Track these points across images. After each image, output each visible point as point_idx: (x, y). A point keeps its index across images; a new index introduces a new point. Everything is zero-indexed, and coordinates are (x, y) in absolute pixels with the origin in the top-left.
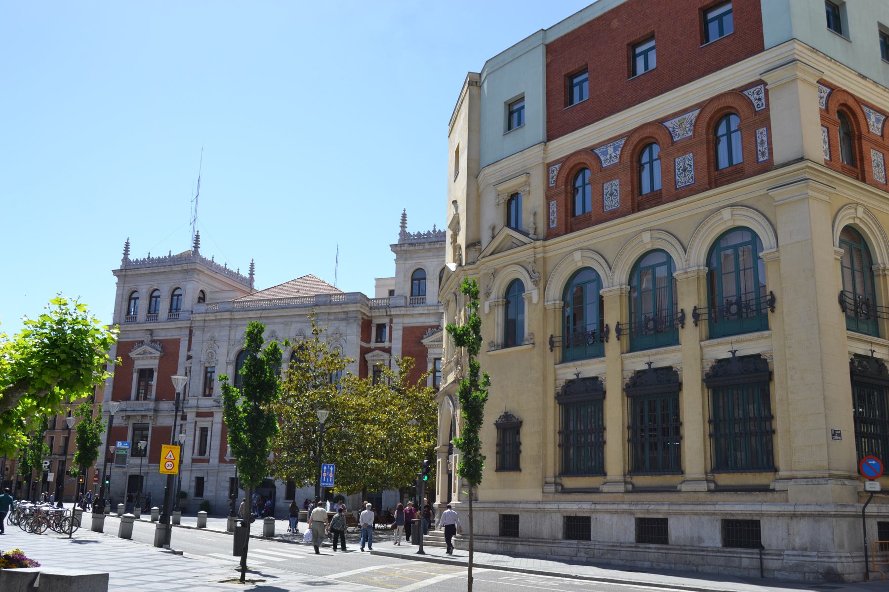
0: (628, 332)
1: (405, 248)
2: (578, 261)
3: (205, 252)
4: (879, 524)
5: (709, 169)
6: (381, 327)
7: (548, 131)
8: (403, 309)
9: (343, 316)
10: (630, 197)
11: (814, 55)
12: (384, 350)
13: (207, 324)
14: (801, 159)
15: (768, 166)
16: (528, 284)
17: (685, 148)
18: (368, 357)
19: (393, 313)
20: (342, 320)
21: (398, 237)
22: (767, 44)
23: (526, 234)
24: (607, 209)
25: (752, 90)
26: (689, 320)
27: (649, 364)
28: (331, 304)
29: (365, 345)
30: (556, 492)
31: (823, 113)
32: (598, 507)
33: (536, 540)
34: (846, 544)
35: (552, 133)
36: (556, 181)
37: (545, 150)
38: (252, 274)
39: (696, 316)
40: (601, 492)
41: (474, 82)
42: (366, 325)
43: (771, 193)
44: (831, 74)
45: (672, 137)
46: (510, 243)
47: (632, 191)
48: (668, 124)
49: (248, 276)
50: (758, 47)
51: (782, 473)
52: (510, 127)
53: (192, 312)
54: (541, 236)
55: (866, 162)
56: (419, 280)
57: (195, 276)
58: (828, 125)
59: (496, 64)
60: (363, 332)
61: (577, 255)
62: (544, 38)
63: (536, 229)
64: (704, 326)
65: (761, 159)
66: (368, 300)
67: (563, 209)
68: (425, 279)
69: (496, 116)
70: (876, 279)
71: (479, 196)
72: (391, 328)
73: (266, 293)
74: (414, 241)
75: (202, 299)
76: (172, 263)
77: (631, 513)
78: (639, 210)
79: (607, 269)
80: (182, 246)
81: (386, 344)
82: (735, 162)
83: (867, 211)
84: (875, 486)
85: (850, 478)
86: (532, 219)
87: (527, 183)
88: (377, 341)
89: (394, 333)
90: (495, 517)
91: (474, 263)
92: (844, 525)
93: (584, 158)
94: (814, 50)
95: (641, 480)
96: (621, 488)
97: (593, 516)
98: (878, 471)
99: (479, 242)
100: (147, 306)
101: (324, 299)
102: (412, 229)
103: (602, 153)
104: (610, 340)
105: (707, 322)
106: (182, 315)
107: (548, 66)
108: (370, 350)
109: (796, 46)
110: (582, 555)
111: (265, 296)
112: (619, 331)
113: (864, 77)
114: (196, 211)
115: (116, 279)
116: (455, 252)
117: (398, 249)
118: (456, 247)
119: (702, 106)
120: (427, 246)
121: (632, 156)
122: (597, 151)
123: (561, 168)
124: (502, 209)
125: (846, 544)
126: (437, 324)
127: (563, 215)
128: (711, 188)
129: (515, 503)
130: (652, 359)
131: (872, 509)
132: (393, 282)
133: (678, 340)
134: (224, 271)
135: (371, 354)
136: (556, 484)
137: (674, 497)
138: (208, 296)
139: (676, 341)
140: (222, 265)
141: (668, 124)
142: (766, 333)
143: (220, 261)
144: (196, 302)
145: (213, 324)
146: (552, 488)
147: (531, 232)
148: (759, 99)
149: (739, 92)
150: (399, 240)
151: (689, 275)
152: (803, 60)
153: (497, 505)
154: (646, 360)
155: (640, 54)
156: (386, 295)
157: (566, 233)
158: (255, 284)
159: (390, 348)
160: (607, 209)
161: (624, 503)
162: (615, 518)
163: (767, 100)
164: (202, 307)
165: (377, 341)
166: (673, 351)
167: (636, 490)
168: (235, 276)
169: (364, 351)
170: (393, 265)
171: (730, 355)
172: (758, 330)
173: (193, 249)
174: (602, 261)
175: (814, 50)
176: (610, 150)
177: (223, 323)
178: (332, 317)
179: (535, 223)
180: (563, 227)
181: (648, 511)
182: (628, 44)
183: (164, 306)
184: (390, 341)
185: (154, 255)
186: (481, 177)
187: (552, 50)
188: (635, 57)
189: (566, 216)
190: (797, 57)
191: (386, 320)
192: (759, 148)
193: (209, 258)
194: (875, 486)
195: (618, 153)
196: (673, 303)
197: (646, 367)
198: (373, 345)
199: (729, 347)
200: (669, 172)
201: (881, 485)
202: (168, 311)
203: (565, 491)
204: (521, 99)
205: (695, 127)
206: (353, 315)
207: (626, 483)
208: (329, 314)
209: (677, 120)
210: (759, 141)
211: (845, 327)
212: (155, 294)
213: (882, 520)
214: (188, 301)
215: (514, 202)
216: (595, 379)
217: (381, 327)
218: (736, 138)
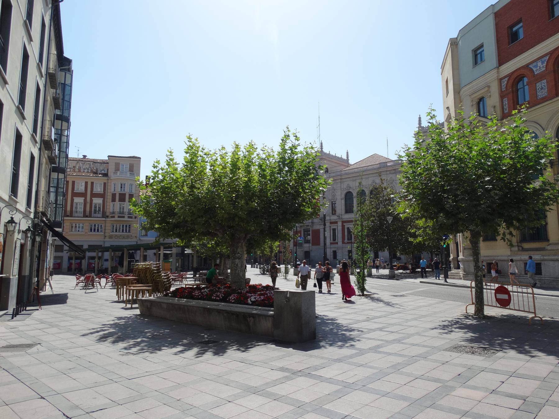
3: (326, 150)
7: (499, 61)
9: (394, 172)
20: (393, 173)
28: (387, 166)
30: (519, 250)
36: (506, 87)
38: (348, 157)
40: (547, 250)
41: (454, 43)
49: (346, 158)
52: (476, 63)
59: (464, 32)
74: (426, 130)
97: (543, 262)
101: (383, 165)
103: (534, 67)
111: (355, 166)
114: (319, 132)
122: (531, 66)
123: (509, 80)
134: (335, 157)
136: (518, 246)
138: (329, 170)
140: (334, 155)
143: (333, 153)
146: (516, 249)
168: (341, 159)
174: (538, 126)
178: (388, 173)
186: (461, 93)
193: (328, 152)
195: (545, 64)
204: (482, 46)
208: (386, 171)
215: (481, 103)
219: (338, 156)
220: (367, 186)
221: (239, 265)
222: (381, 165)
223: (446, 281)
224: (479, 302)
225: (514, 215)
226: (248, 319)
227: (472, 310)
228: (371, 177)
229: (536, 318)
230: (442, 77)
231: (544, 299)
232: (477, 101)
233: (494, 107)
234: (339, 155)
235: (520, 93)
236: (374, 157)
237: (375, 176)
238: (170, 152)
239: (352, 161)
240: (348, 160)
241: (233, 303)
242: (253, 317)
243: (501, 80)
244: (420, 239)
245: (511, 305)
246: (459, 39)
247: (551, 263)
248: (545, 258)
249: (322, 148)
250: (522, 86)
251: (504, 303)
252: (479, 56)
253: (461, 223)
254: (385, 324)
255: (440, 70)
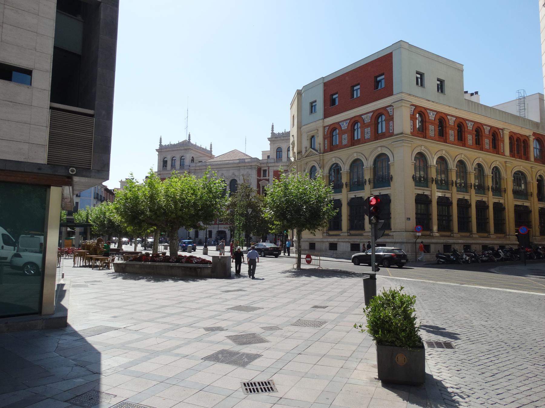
0: (349, 185)
1: (274, 139)
2: (334, 161)
3: (193, 141)
4: (482, 246)
5: (375, 133)
6: (265, 171)
7: (324, 115)
8: (273, 164)
9: (250, 167)
10: (350, 140)
11: (409, 96)
12: (266, 180)
13: (196, 171)
14: (402, 133)
15: (392, 135)
16: (318, 168)
17: (368, 126)
18: (260, 183)
19: (269, 165)
20: (250, 169)
21: (271, 135)
22: (394, 93)
23: (317, 151)
24: (343, 144)
25: (389, 108)
26: (367, 183)
27: (355, 196)
28: (245, 162)
29: (259, 178)
30: (327, 235)
31: (412, 116)
32: (339, 240)
33: (321, 251)
34: (410, 251)
35: (326, 116)
36: (327, 133)
37: (323, 122)
38: (211, 149)
39: (369, 181)
40: (341, 236)
41: (299, 93)
42: (259, 170)
43: (393, 143)
44: (415, 101)
45: (364, 121)
46: (312, 153)
47: (351, 138)
48: (363, 117)
49: (209, 149)
50: (391, 94)
51: (392, 230)
52: (311, 112)
53: (190, 166)
54: (322, 152)
55: (427, 130)
56: (279, 152)
57: (190, 151)
58: (413, 119)
59: (307, 88)
60: (258, 173)
61: (334, 159)
62: (323, 80)
63: (320, 149)
64: (372, 184)
65: (391, 132)
66: (260, 160)
67: (329, 143)
68: (282, 151)
69: (307, 107)
70: (428, 169)
71: (301, 135)
72: (269, 171)
73: (219, 158)
74: (277, 136)
75: (193, 160)
76: (180, 146)
77: (349, 242)
78: (353, 146)
79: (343, 164)
80: (182, 138)
81: (267, 178)
82: (383, 132)
83: (425, 147)
84: (420, 234)
85: (413, 232)
86: (319, 146)
87: (317, 133)
88: (263, 177)
89: (270, 173)
90: (308, 244)
91: (300, 159)
92: (409, 246)
93: (336, 126)
94: (410, 95)
95: (353, 232)
96: (346, 234)
97: (338, 243)
98: (420, 230)
99: (301, 152)
100: (171, 164)
101: (242, 161)
102: (276, 131)
103: (342, 124)
104: (344, 188)
105: (373, 183)
106: (185, 167)
107: (325, 91)
108: (261, 180)
109: (403, 95)
110: (335, 255)
111: (218, 159)
112: (346, 185)
113: (429, 101)
114: (187, 124)
115: (157, 153)
116: (293, 154)
117: (271, 140)
118: (294, 153)
119: (374, 112)
120: (282, 138)
121: (351, 126)
122: (340, 124)
123: (329, 128)
124: (309, 141)
125: (410, 251)
126: (287, 169)
127: (329, 145)
128: (375, 140)
129: (314, 239)
130: (356, 194)
131: (419, 240)
132: (269, 152)
133: (364, 188)
134: (200, 148)
135: (261, 182)
136: (327, 233)
137: (362, 237)
138: (195, 159)
139: (363, 189)
140: (200, 146)
141: (363, 117)
142: (390, 187)
143: (199, 145)
144: (191, 162)
145: (198, 171)
146: (326, 234)
147: (319, 150)
148: (391, 111)
149: (385, 108)
150: (271, 136)
151: (368, 168)
152: (405, 99)
153: (308, 240)
154: (354, 194)
155: (355, 90)
156: (266, 158)
157: (330, 151)
158: (212, 152)
159: (269, 179)
160: (343, 144)
161: (347, 239)
162: (345, 244)
163: (393, 112)
164: (193, 165)
165: (263, 177)
166: (363, 192)
167: (351, 235)
168: (205, 150)
169: (259, 181)
170: (269, 146)
171: (379, 194)
172: (388, 187)
173: (188, 140)
174: (341, 161)
175: (410, 95)
176: (345, 124)
177: (202, 170)
178: (246, 168)
179: (320, 147)
180: (329, 150)
181: (354, 242)
182: (351, 86)
183: (178, 164)
184: (269, 176)
185: (173, 143)
186: (302, 129)
187: (326, 84)
188: (353, 91)
189: (330, 145)
190: (403, 98)
191: (267, 168)
192: (390, 128)
193: (194, 144)
194: (420, 234)
195: (347, 125)
196: (363, 177)
197: (354, 197)
198: (262, 178)
199: (379, 192)
200: (363, 133)
201: (422, 234)
202: (179, 166)
203: (330, 235)
204: (315, 101)
205: (371, 118)
206: (254, 166)
207: (348, 232)
208: (244, 166)
209: (366, 115)
210: (390, 125)
211: (414, 185)
212: (174, 159)
213: (445, 244)
214: (187, 162)
215: (313, 139)
216: (339, 200)
217: (265, 171)
218: (384, 123)
219: (203, 147)
220: (228, 177)
221: (176, 243)
222: (241, 160)
223: (284, 255)
224: (299, 263)
225: (314, 223)
226: (197, 270)
227: (295, 266)
228: (232, 170)
229: (320, 268)
230: (291, 112)
231: (336, 263)
232: (310, 137)
233: (320, 144)
234: (203, 147)
235: (334, 137)
236: (234, 152)
237: (235, 170)
238: (131, 174)
239: (216, 153)
240: (211, 151)
241: (185, 263)
242: (200, 269)
243: (324, 127)
244: (274, 231)
245: (312, 263)
246: (303, 91)
247: (342, 243)
248: (339, 240)
249: (189, 139)
250: (335, 134)
251: (309, 262)
252: (314, 107)
253: (293, 225)
254: (222, 304)
255: (290, 106)
